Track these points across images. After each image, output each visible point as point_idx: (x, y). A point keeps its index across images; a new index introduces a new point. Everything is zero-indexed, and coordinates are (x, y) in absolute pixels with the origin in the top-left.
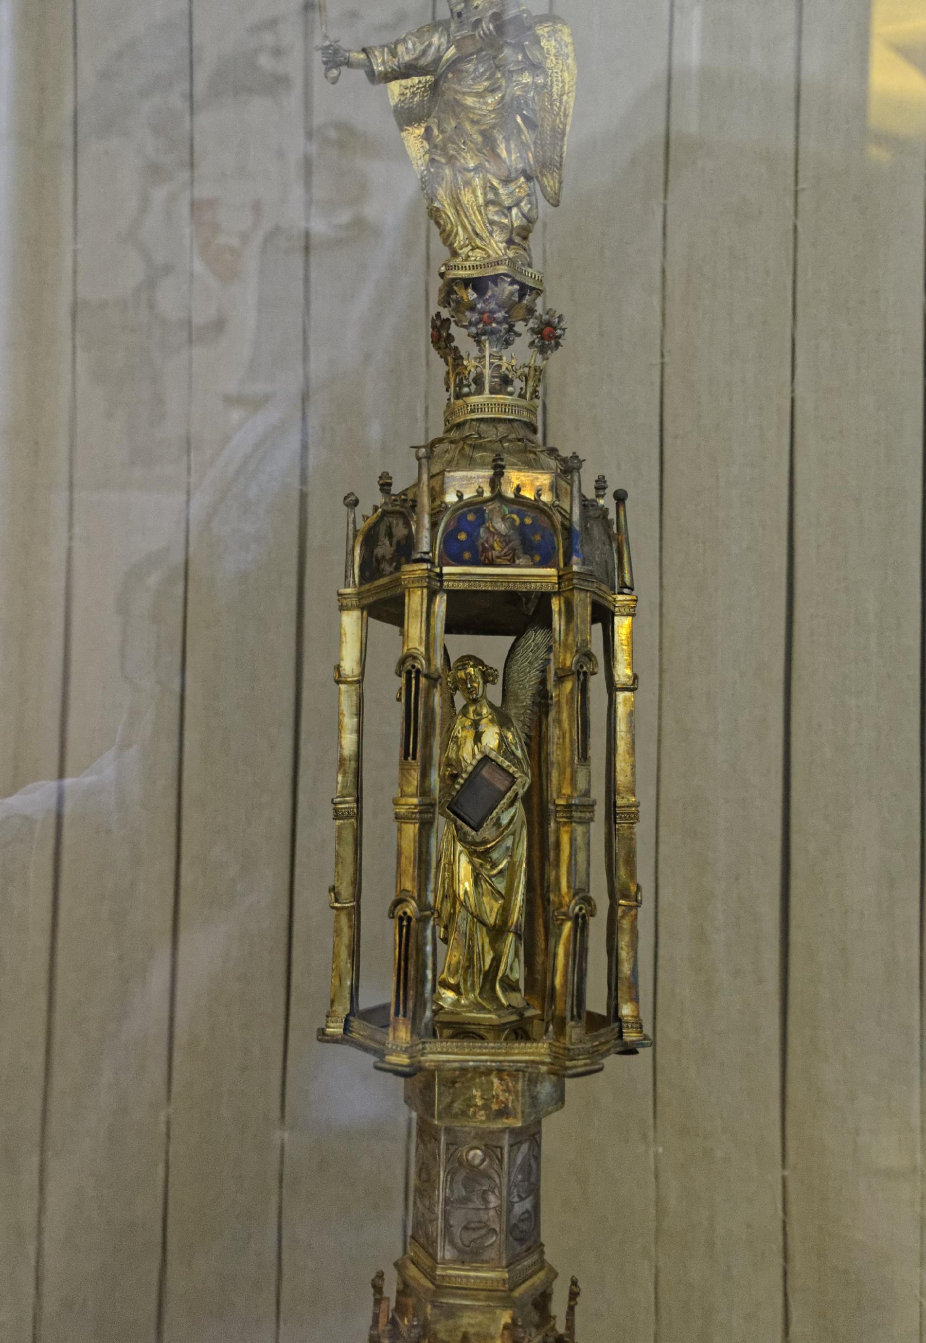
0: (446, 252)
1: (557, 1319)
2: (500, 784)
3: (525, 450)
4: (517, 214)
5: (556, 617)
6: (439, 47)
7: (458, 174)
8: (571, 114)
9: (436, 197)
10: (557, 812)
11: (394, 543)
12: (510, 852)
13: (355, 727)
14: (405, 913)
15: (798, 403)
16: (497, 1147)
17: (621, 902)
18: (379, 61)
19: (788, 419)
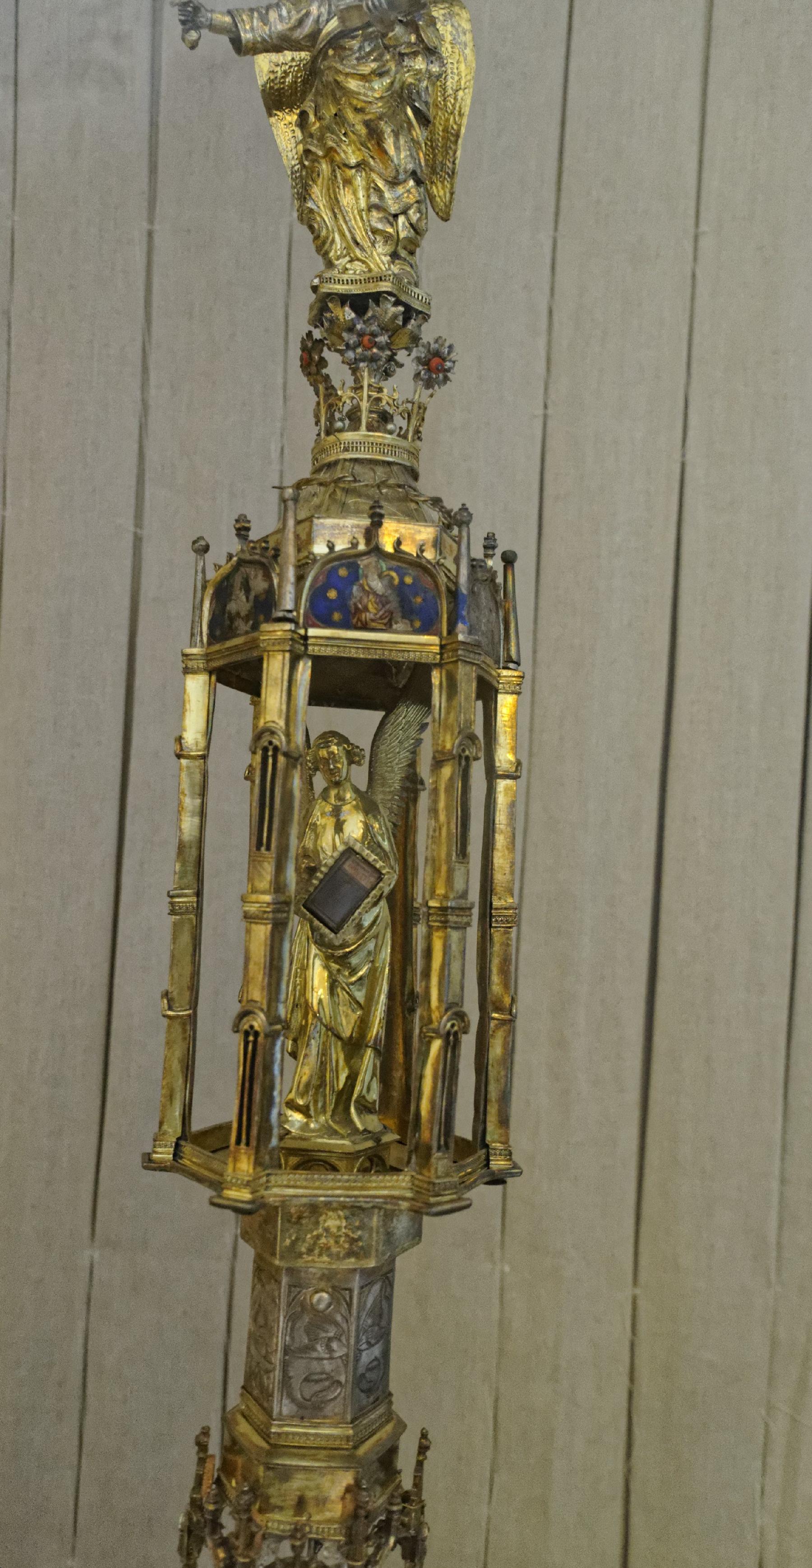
0: (320, 264)
1: (402, 1474)
2: (366, 881)
3: (406, 499)
4: (404, 223)
5: (436, 692)
6: (319, 17)
7: (337, 170)
8: (467, 113)
9: (310, 195)
10: (429, 914)
11: (252, 597)
12: (371, 958)
13: (198, 810)
14: (252, 1027)
15: (688, 469)
16: (346, 1289)
17: (495, 1015)
18: (248, 27)
19: (676, 486)
